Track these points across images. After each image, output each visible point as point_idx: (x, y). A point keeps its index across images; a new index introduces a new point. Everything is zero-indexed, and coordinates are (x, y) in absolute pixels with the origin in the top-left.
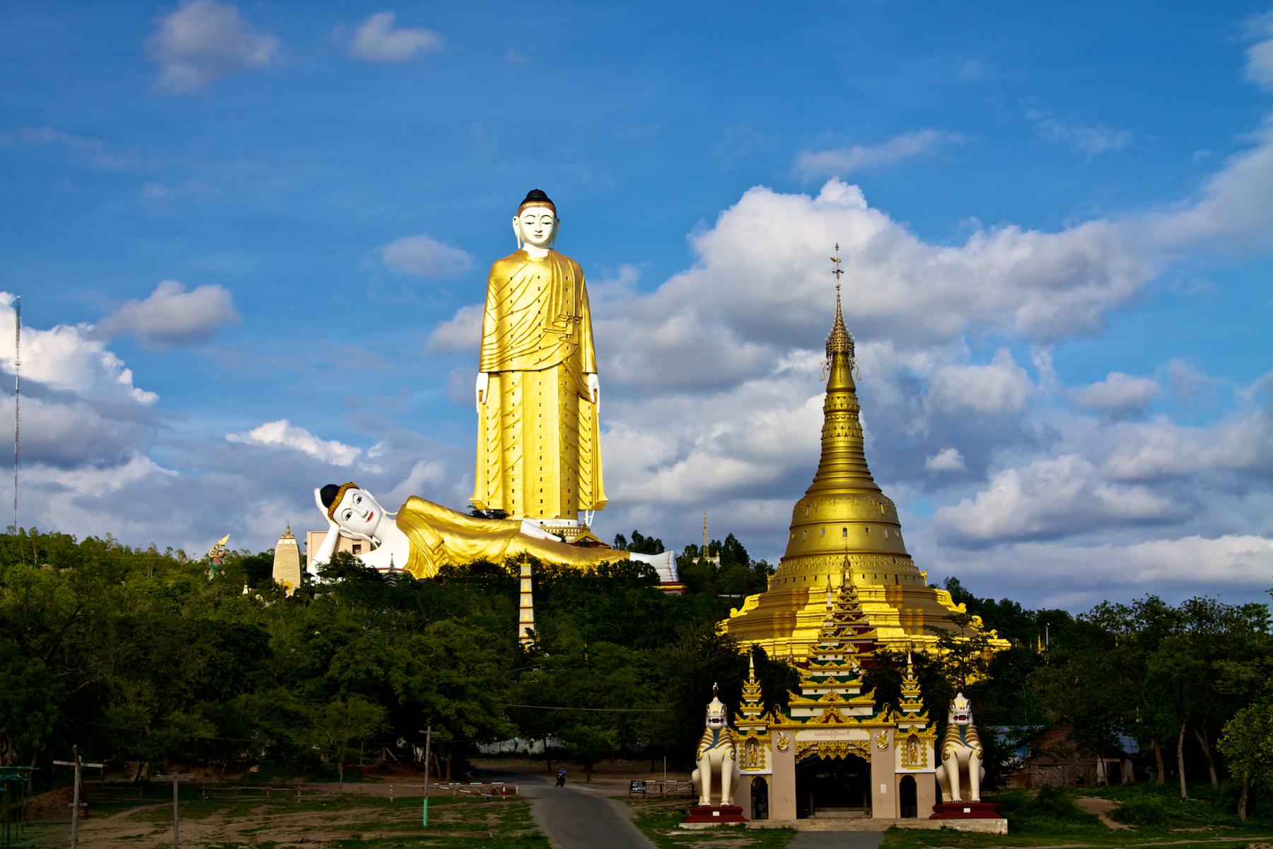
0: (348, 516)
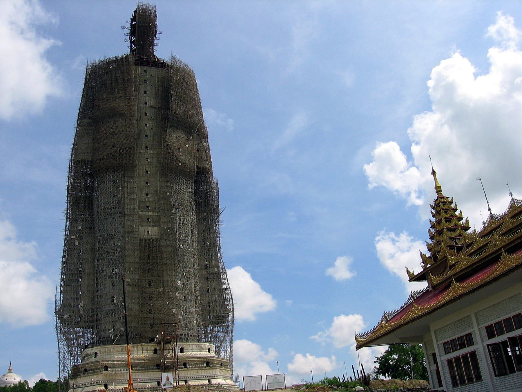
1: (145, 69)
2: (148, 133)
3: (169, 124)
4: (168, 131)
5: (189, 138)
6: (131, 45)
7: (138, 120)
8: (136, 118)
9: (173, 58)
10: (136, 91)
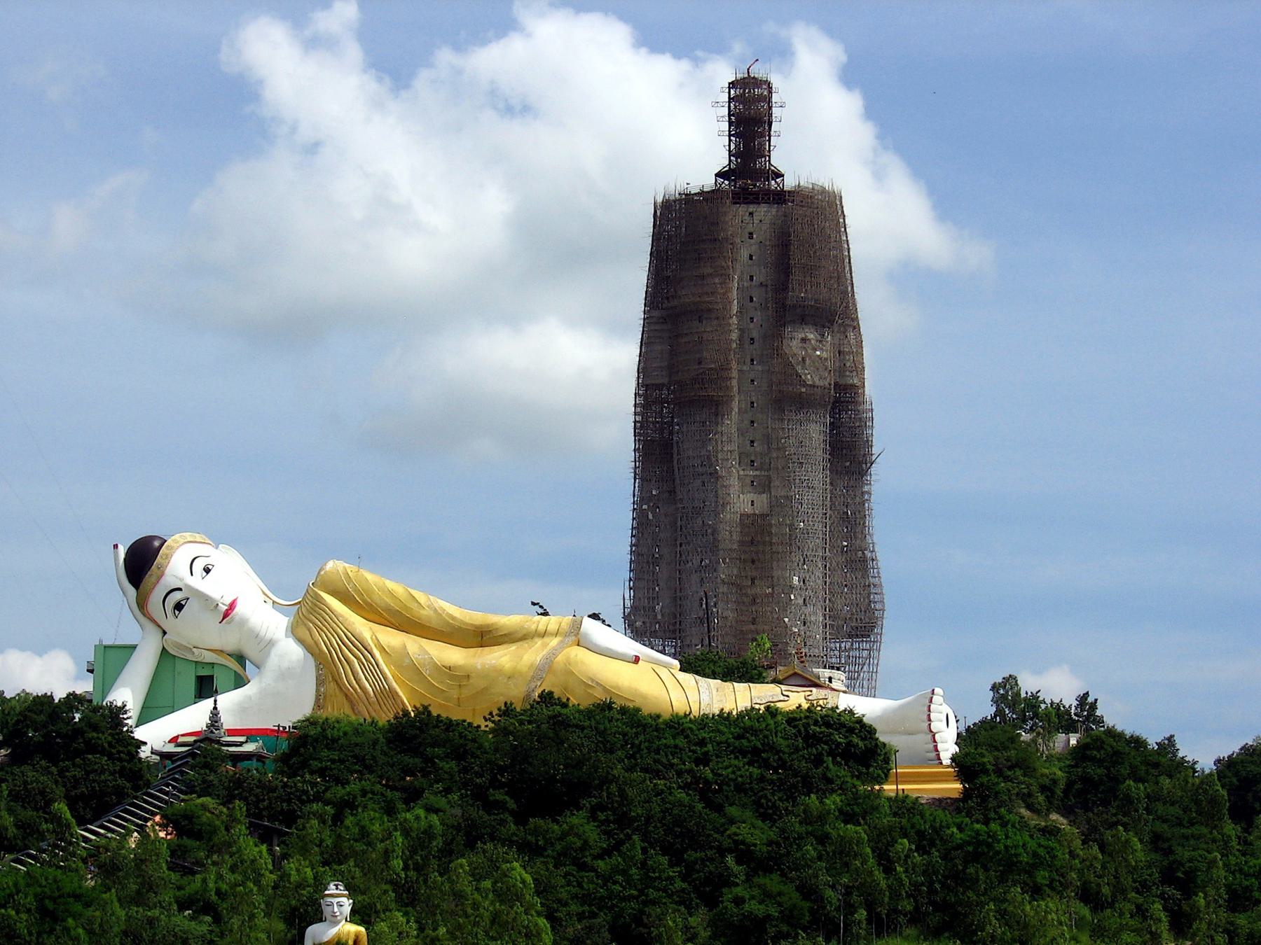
0: (179, 607)
2: (755, 334)
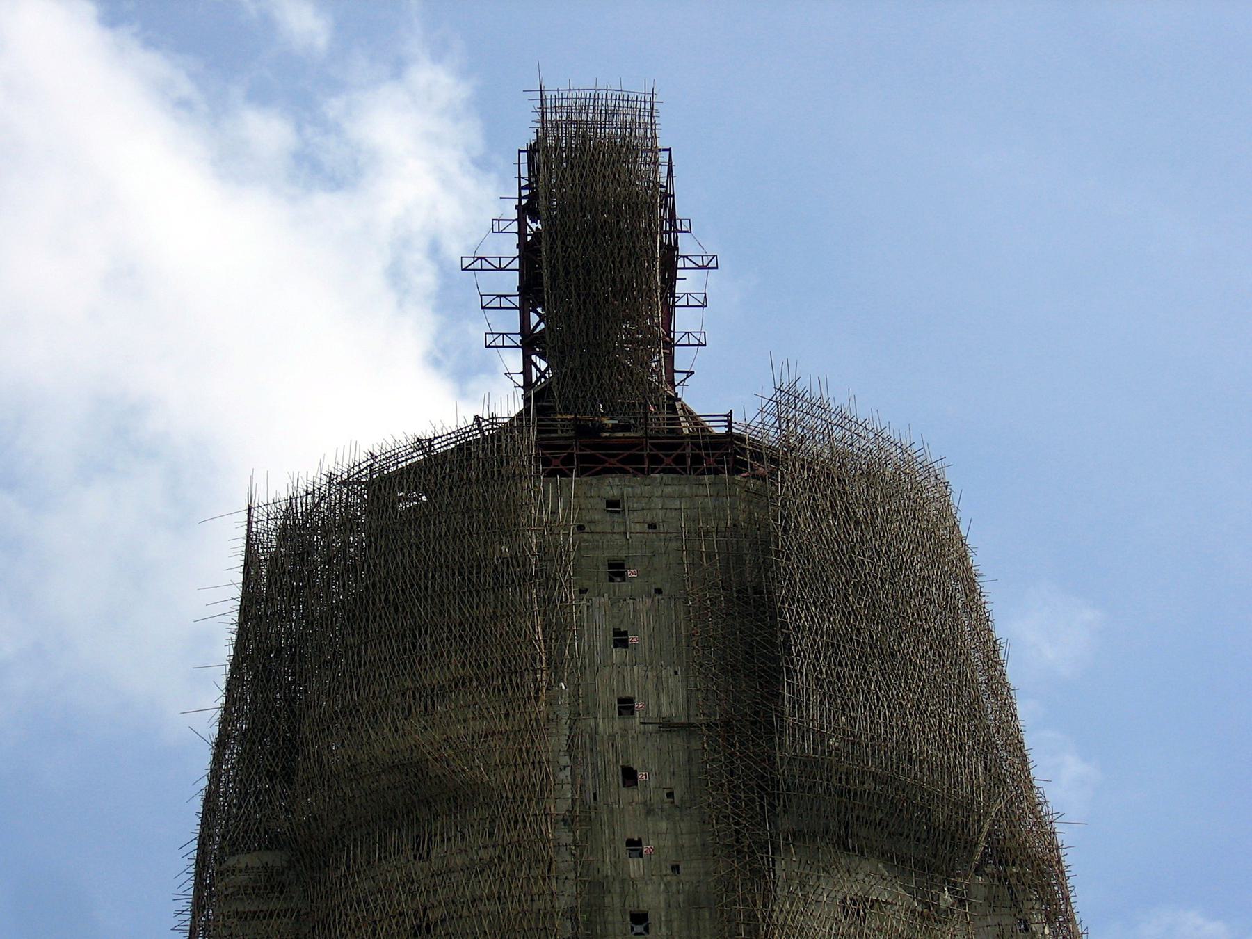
1: (614, 493)
2: (652, 899)
3: (785, 823)
4: (784, 867)
5: (930, 904)
6: (528, 363)
7: (582, 817)
8: (563, 807)
9: (786, 397)
10: (556, 633)
